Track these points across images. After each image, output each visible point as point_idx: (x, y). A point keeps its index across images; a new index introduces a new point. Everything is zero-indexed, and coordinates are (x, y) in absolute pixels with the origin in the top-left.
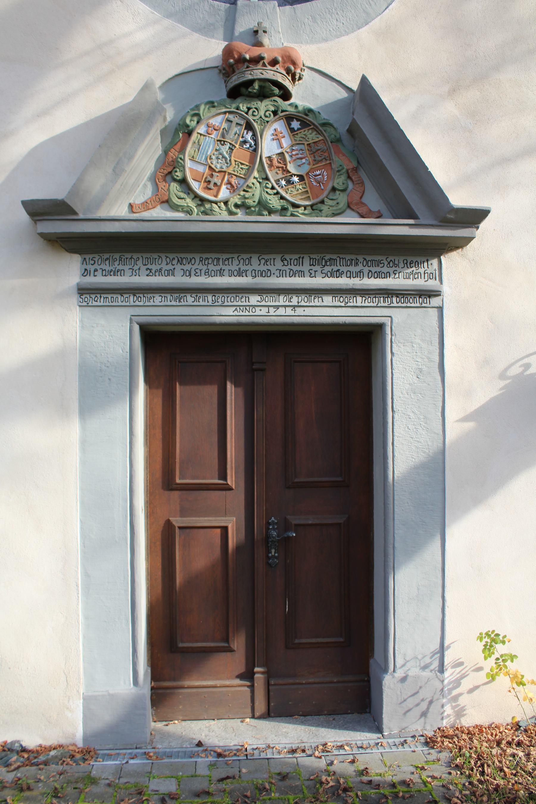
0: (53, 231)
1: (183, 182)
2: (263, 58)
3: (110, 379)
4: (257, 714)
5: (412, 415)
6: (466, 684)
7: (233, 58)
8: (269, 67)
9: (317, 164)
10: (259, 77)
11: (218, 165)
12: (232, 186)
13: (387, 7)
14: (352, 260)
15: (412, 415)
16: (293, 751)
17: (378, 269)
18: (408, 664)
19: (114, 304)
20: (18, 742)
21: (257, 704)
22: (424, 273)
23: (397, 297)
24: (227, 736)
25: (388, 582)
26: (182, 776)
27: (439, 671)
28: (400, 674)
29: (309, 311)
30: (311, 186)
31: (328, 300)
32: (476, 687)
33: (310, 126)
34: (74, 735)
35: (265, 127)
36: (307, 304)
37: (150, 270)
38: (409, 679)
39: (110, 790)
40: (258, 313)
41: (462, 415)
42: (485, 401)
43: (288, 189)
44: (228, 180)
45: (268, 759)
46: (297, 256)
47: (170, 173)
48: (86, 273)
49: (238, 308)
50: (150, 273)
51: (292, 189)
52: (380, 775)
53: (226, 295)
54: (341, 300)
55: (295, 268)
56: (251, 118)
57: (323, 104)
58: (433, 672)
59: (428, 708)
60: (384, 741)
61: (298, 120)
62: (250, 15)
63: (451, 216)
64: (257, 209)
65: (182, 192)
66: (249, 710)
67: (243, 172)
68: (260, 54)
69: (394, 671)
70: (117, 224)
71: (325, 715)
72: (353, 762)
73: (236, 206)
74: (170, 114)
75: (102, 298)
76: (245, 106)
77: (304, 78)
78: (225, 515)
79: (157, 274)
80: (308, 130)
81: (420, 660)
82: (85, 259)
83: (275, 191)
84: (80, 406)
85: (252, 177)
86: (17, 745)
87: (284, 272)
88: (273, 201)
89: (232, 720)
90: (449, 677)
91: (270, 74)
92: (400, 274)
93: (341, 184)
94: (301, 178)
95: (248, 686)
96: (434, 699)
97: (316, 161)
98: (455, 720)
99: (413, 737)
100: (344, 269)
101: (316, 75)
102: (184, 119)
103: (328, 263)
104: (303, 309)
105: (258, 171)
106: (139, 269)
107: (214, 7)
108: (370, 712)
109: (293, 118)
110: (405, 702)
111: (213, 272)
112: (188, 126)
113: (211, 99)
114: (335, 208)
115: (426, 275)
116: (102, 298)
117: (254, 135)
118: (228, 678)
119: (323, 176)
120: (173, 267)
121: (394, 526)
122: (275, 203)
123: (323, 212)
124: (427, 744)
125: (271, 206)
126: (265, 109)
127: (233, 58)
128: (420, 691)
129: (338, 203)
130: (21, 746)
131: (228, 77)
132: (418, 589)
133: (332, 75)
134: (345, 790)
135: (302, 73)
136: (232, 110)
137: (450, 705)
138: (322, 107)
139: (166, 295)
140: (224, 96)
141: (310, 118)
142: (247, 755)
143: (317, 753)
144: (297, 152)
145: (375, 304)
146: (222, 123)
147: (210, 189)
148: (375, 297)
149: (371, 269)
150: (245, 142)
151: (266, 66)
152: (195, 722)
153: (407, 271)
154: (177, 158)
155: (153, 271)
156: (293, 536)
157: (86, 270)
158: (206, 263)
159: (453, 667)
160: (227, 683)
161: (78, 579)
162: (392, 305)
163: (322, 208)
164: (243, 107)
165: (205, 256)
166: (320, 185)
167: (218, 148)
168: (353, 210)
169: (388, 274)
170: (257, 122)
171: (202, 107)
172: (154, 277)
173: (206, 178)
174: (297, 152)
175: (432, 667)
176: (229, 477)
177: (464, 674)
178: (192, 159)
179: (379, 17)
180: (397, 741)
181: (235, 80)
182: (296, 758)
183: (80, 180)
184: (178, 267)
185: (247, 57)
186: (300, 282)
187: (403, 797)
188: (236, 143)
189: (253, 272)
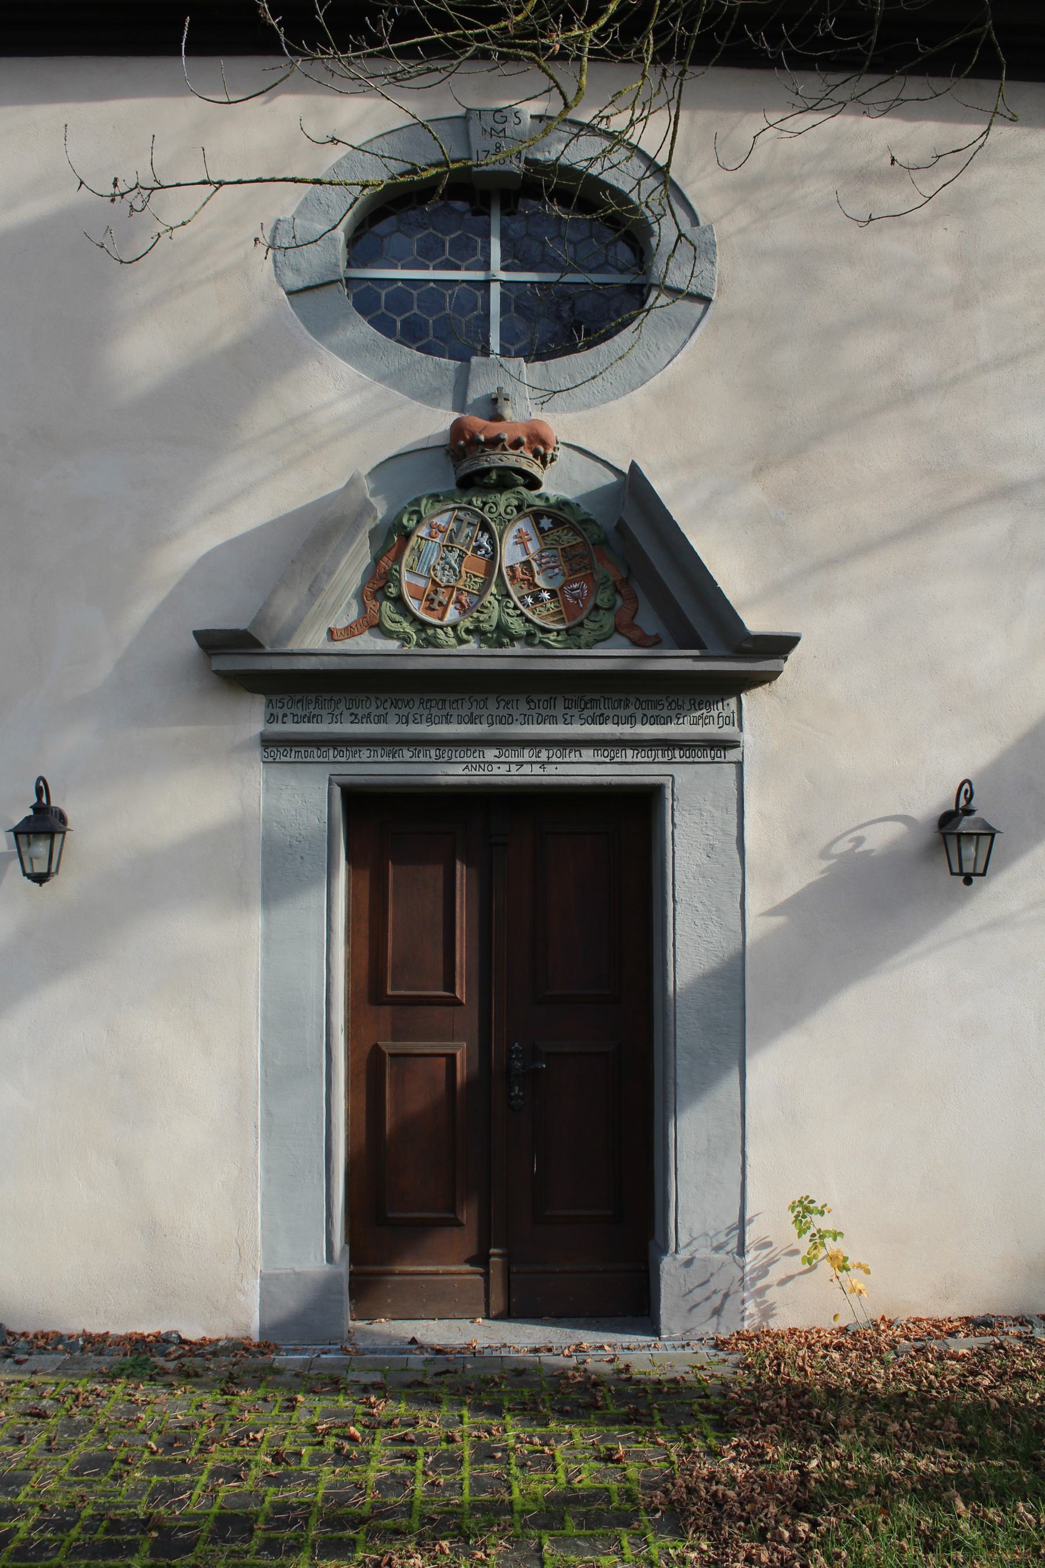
0: (232, 668)
1: (399, 601)
2: (503, 440)
3: (302, 858)
4: (493, 1313)
5: (700, 907)
6: (776, 1273)
7: (464, 439)
8: (511, 451)
9: (573, 574)
10: (496, 465)
11: (443, 578)
12: (462, 606)
13: (671, 360)
14: (621, 700)
15: (700, 907)
16: (536, 1350)
17: (655, 713)
18: (694, 1242)
19: (309, 759)
20: (176, 1332)
21: (493, 1298)
22: (718, 717)
23: (681, 749)
24: (451, 1335)
25: (668, 1130)
26: (389, 1370)
27: (738, 1254)
28: (684, 1255)
29: (562, 769)
30: (566, 604)
31: (588, 754)
32: (790, 1278)
33: (565, 524)
34: (248, 1326)
35: (506, 527)
36: (560, 760)
37: (356, 716)
38: (696, 1263)
39: (298, 1380)
40: (496, 771)
41: (768, 906)
42: (801, 888)
43: (535, 608)
44: (457, 598)
45: (502, 1357)
46: (547, 697)
47: (382, 588)
48: (271, 719)
49: (470, 765)
50: (355, 719)
51: (541, 609)
52: (645, 1373)
53: (453, 749)
54: (606, 755)
55: (544, 712)
56: (487, 516)
57: (584, 492)
58: (730, 1254)
59: (722, 1304)
60: (660, 1344)
61: (549, 517)
62: (488, 376)
63: (748, 645)
64: (495, 635)
65: (397, 613)
66: (482, 1308)
67: (477, 587)
68: (499, 435)
69: (676, 1251)
70: (313, 658)
71: (587, 1317)
72: (611, 1361)
73: (468, 631)
74: (381, 509)
75: (293, 752)
76: (480, 499)
77: (558, 459)
78: (452, 1038)
79: (364, 720)
80: (563, 530)
81: (711, 1238)
82: (271, 700)
83: (518, 612)
84: (263, 891)
85: (489, 593)
86: (174, 1335)
87: (530, 717)
88: (516, 625)
89: (458, 1321)
90: (750, 1262)
91: (511, 459)
92: (686, 718)
93: (606, 600)
94: (553, 594)
95: (481, 1274)
96: (731, 1293)
97: (573, 571)
98: (760, 1322)
99: (701, 1340)
100: (608, 712)
101: (576, 454)
102: (399, 517)
103: (589, 706)
104: (555, 766)
105: (497, 586)
106: (341, 714)
107: (440, 366)
108: (649, 1315)
109: (543, 514)
110: (691, 1294)
111: (437, 718)
112: (405, 527)
113: (435, 491)
114: (598, 633)
115: (721, 719)
116: (293, 752)
117: (492, 538)
118: (454, 1263)
119: (582, 589)
120: (386, 711)
121: (675, 1055)
122: (517, 626)
123: (582, 637)
124: (716, 1346)
125: (513, 631)
126: (506, 504)
127: (464, 439)
128: (711, 1280)
129: (601, 626)
130: (179, 1337)
131: (458, 460)
132: (709, 1141)
133: (595, 454)
134: (595, 1384)
135: (555, 453)
136: (463, 505)
137: (753, 1300)
138: (582, 497)
139: (375, 748)
140: (453, 487)
141: (565, 514)
142: (474, 1353)
143: (566, 1352)
144: (548, 559)
145: (651, 760)
146: (449, 523)
147: (434, 610)
148: (651, 750)
149: (645, 712)
150: (479, 547)
151: (506, 450)
152: (409, 1321)
153: (694, 715)
154: (391, 569)
155: (359, 717)
156: (542, 1068)
157: (272, 715)
158: (428, 707)
159: (757, 1249)
160: (453, 1268)
161: (257, 1118)
162: (674, 760)
163: (581, 633)
164: (477, 502)
165: (426, 697)
166: (578, 602)
167: (444, 556)
168: (622, 634)
169: (669, 719)
170: (495, 521)
171: (424, 502)
172: (360, 725)
173: (428, 595)
174: (548, 559)
175: (729, 1248)
176: (458, 988)
177: (773, 1258)
178: (411, 569)
179: (660, 374)
180: (677, 1343)
181: (468, 467)
182: (539, 1357)
183: (267, 604)
184: (392, 711)
185: (482, 438)
186: (551, 731)
187: (668, 1393)
188: (468, 549)
189: (490, 717)
